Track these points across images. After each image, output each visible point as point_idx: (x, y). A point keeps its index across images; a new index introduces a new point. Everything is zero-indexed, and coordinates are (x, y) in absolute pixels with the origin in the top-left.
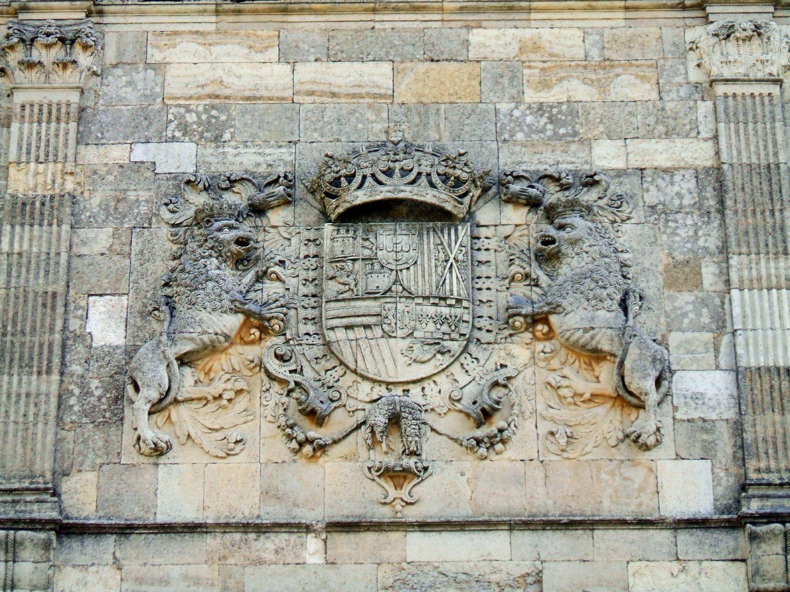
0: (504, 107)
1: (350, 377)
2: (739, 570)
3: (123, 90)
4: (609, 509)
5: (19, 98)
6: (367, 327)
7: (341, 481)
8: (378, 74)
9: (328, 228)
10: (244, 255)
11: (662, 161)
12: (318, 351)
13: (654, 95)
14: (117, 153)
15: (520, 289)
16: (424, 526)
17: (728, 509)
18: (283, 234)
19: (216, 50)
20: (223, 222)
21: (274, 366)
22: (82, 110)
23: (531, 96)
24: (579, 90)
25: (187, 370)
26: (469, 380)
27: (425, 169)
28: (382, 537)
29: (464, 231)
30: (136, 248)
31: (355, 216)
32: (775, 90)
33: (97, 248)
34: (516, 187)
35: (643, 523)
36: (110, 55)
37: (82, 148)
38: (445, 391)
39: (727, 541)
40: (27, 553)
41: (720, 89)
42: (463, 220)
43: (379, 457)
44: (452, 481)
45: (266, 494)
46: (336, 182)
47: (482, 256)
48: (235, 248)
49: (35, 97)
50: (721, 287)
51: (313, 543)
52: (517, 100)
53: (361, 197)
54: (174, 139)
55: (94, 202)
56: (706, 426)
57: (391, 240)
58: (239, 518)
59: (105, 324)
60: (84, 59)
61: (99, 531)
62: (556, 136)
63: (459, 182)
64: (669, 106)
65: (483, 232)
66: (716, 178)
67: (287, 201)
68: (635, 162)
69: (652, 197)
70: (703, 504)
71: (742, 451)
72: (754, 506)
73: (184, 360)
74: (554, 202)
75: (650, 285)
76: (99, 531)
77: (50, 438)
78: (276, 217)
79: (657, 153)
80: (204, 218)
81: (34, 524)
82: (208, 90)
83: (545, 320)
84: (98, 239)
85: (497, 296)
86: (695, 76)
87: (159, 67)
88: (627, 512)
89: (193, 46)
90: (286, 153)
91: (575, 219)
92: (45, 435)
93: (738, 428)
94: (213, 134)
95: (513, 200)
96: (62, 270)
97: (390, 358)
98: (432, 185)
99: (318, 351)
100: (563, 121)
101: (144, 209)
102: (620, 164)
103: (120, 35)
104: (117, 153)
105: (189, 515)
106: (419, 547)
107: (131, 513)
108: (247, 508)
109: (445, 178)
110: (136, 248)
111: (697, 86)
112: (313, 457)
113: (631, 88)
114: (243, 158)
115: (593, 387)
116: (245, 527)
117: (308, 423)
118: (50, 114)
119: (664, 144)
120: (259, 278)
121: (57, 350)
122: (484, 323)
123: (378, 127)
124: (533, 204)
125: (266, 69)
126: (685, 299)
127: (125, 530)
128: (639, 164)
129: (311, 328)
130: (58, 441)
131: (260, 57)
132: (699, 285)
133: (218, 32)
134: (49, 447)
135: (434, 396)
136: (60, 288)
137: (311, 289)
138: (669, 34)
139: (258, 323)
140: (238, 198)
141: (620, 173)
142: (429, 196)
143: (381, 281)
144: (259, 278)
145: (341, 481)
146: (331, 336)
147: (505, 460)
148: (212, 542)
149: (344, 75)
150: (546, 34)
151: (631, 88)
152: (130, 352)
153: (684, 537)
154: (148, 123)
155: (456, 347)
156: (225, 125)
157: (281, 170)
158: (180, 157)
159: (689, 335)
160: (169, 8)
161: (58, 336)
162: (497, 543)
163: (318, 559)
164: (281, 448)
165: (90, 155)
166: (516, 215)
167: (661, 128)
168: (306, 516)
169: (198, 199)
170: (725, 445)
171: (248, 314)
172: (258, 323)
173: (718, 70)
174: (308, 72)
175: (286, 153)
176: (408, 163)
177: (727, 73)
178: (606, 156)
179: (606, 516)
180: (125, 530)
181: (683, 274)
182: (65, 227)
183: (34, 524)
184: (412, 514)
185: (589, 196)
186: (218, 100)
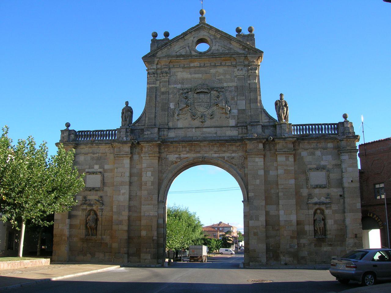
0: (214, 79)
1: (198, 250)
2: (237, 131)
3: (173, 79)
4: (224, 125)
5: (162, 80)
6: (199, 106)
7: (197, 123)
8: (200, 75)
9: (195, 94)
10: (186, 98)
11: (231, 85)
12: (194, 108)
13: (230, 77)
14: (172, 86)
15: (215, 101)
16: (205, 128)
17: (236, 125)
18: (190, 95)
19: (183, 73)
20: (185, 93)
21: (189, 110)
22: (169, 81)
23: (217, 78)
24: (222, 77)
25: (180, 111)
26: (210, 111)
27: (205, 88)
28: (201, 129)
29: (209, 94)
30: (175, 97)
31: (198, 93)
32: (243, 77)
33: (171, 97)
34: (215, 89)
35: (227, 127)
36: (171, 75)
37: (169, 86)
38: (208, 112)
39: (237, 129)
40: (165, 131)
41: (238, 77)
42: (209, 93)
43: (201, 120)
44: (208, 122)
45: (189, 124)
46: (196, 89)
47: (211, 97)
48: (185, 97)
49: (164, 80)
50: (237, 100)
51: (194, 129)
52: (215, 78)
53: (199, 91)
54: (178, 84)
55: (170, 92)
56: (234, 116)
57: (202, 96)
58: (186, 127)
59: (172, 106)
60: (168, 75)
61: (172, 129)
62: (220, 83)
63: (209, 89)
64: (232, 79)
65: (212, 94)
66: (236, 87)
67: (191, 91)
68: (228, 85)
69: (230, 90)
70: (234, 124)
71: (238, 119)
72: (239, 125)
73: (180, 110)
74: (220, 90)
75: (229, 100)
76: (172, 129)
77: (167, 119)
78: (190, 93)
79: (230, 84)
80: (182, 94)
81: (166, 128)
82: (182, 78)
83: (218, 104)
84: (171, 96)
85: (213, 101)
86: (235, 75)
87: (177, 76)
88: (226, 126)
89: (180, 73)
90: (190, 85)
91: (221, 93)
92: (166, 118)
93: (238, 116)
94: (182, 83)
95: (215, 91)
96: (167, 100)
97: (202, 109)
98: (206, 90)
99: (194, 108)
100: (220, 81)
101: (176, 92)
102: (226, 86)
103: (172, 72)
104: (172, 86)
105: (181, 127)
106: (204, 130)
107: (176, 127)
108: (187, 126)
109: (207, 89)
110: (175, 97)
111: (235, 76)
112: (194, 120)
113: (228, 77)
114: (186, 86)
115: (223, 112)
116: (187, 128)
117: (193, 116)
118: (165, 82)
119: (231, 83)
120: (188, 100)
121: (167, 109)
122: (212, 105)
123: (200, 82)
124: (217, 91)
125: (188, 75)
126: (233, 101)
127: (175, 129)
128: (229, 86)
129: (193, 106)
130: (168, 119)
131: (188, 74)
132: (234, 100)
133: (183, 71)
134: (167, 120)
135: (206, 113)
136: (167, 102)
137: (193, 101)
138: (232, 70)
139: (187, 106)
140: (185, 91)
141: (227, 87)
142: (206, 91)
143: (201, 101)
144: (188, 100)
145: (197, 123)
146: (195, 107)
147: (213, 120)
148: (184, 129)
149: (197, 76)
150: (219, 70)
151: (228, 77)
152: (175, 109)
153: (232, 128)
154: (176, 82)
155: (208, 108)
156: (184, 82)
157: (190, 87)
158: (179, 86)
159: (233, 106)
160: (344, 272)
161: (167, 108)
162: (213, 129)
163: (195, 131)
164: (190, 119)
165: (170, 86)
166: (215, 92)
167: (231, 81)
168: (193, 126)
169: (181, 91)
170: (236, 118)
171: (187, 105)
172: (187, 106)
173: (237, 74)
174: (193, 75)
175: (190, 85)
176: (203, 87)
177: (239, 75)
178: (225, 85)
179: (224, 126)
180: (175, 129)
181: (233, 99)
182: (167, 95)
183: (166, 128)
184: (204, 126)
185: (223, 90)
186: (183, 79)
